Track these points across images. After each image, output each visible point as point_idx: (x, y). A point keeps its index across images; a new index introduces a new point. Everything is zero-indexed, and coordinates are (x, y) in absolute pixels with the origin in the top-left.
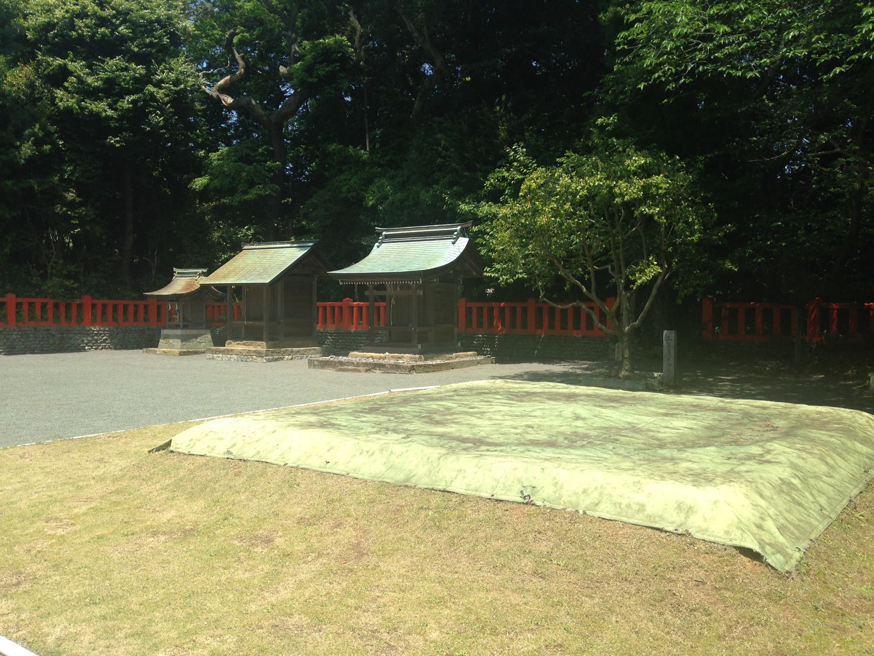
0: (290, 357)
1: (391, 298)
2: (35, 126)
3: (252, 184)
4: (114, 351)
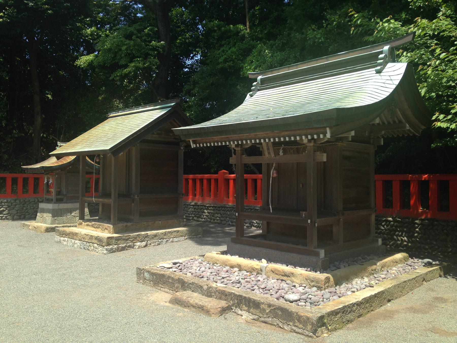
0: (144, 243)
1: (269, 166)
2: (377, 241)
3: (132, 58)
4: (11, 223)
